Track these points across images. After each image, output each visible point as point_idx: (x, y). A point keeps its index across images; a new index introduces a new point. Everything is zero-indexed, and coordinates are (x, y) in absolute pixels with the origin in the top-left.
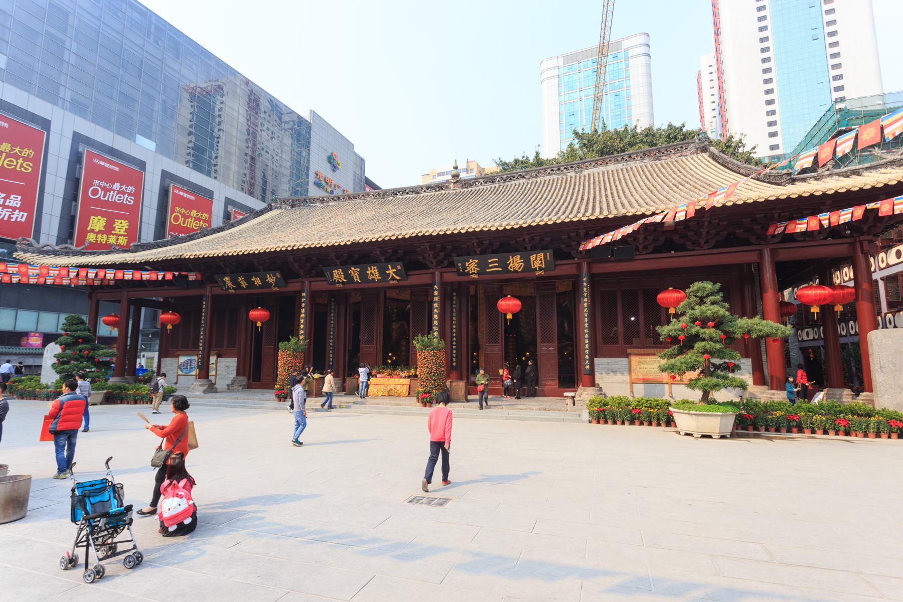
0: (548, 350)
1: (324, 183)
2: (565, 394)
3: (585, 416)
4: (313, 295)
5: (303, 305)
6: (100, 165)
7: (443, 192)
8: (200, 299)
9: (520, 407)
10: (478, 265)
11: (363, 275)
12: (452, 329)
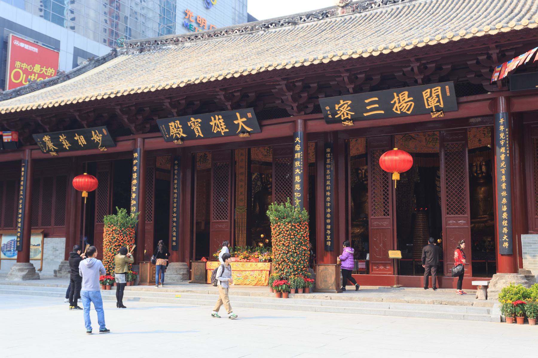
0: (456, 223)
1: (194, 25)
2: (474, 283)
3: (497, 311)
4: (149, 156)
5: (135, 168)
6: (20, 47)
7: (328, 20)
8: (17, 164)
9: (406, 299)
10: (352, 108)
11: (206, 127)
12: (326, 197)
